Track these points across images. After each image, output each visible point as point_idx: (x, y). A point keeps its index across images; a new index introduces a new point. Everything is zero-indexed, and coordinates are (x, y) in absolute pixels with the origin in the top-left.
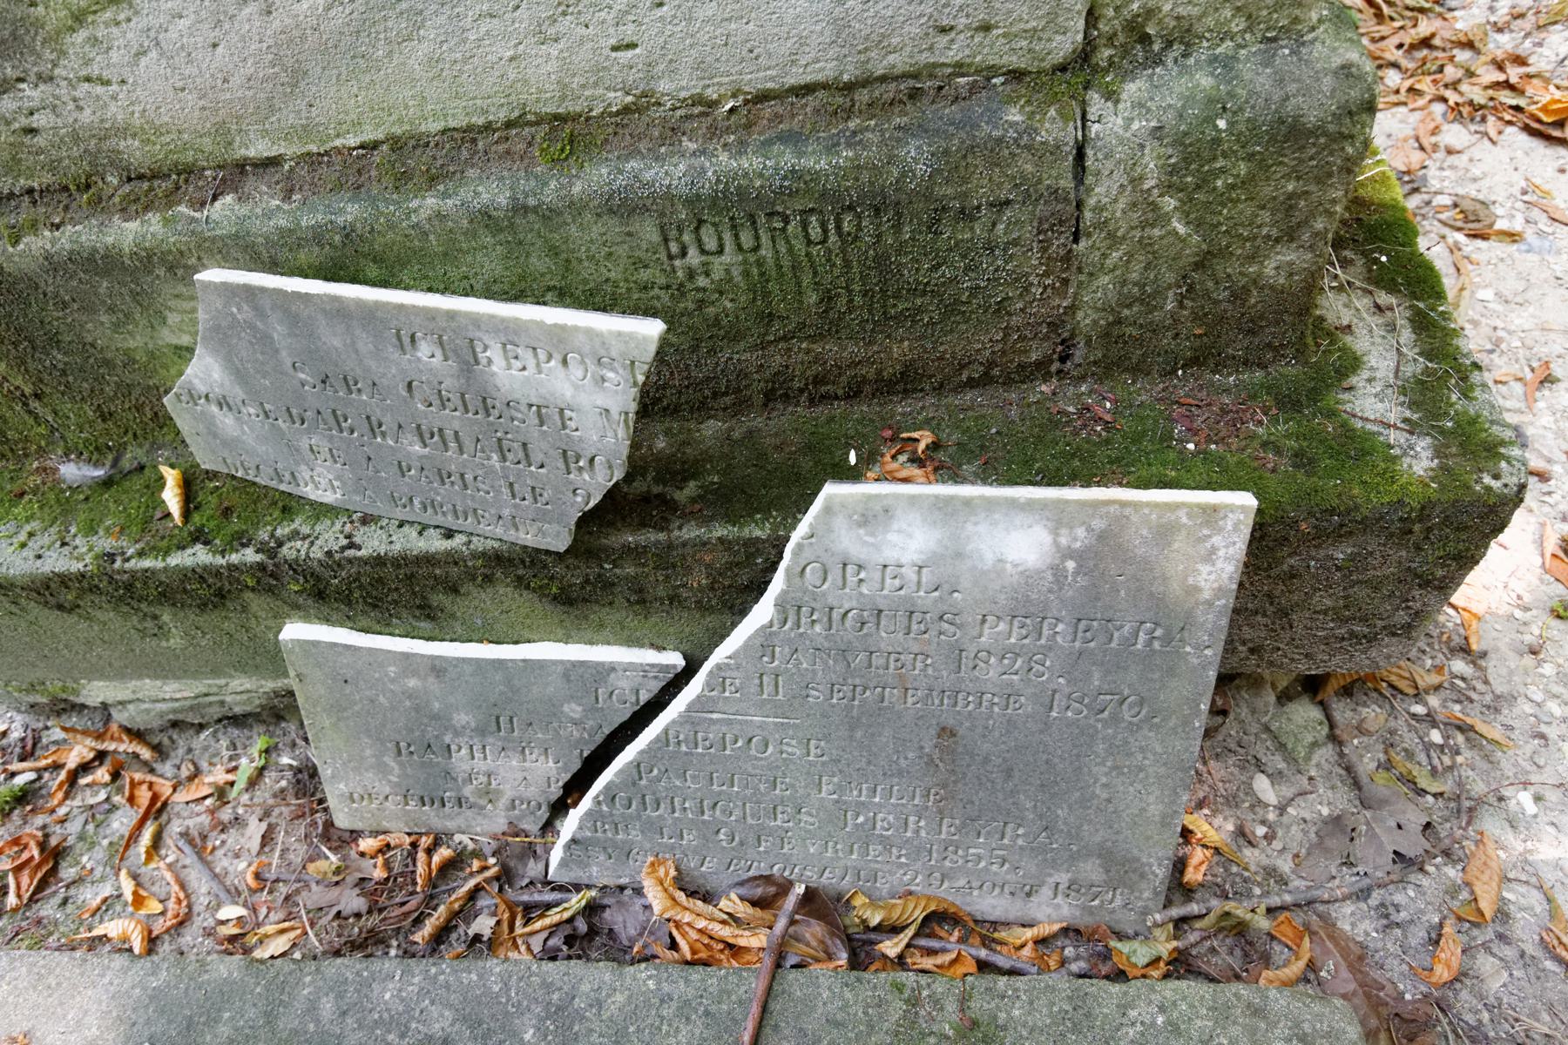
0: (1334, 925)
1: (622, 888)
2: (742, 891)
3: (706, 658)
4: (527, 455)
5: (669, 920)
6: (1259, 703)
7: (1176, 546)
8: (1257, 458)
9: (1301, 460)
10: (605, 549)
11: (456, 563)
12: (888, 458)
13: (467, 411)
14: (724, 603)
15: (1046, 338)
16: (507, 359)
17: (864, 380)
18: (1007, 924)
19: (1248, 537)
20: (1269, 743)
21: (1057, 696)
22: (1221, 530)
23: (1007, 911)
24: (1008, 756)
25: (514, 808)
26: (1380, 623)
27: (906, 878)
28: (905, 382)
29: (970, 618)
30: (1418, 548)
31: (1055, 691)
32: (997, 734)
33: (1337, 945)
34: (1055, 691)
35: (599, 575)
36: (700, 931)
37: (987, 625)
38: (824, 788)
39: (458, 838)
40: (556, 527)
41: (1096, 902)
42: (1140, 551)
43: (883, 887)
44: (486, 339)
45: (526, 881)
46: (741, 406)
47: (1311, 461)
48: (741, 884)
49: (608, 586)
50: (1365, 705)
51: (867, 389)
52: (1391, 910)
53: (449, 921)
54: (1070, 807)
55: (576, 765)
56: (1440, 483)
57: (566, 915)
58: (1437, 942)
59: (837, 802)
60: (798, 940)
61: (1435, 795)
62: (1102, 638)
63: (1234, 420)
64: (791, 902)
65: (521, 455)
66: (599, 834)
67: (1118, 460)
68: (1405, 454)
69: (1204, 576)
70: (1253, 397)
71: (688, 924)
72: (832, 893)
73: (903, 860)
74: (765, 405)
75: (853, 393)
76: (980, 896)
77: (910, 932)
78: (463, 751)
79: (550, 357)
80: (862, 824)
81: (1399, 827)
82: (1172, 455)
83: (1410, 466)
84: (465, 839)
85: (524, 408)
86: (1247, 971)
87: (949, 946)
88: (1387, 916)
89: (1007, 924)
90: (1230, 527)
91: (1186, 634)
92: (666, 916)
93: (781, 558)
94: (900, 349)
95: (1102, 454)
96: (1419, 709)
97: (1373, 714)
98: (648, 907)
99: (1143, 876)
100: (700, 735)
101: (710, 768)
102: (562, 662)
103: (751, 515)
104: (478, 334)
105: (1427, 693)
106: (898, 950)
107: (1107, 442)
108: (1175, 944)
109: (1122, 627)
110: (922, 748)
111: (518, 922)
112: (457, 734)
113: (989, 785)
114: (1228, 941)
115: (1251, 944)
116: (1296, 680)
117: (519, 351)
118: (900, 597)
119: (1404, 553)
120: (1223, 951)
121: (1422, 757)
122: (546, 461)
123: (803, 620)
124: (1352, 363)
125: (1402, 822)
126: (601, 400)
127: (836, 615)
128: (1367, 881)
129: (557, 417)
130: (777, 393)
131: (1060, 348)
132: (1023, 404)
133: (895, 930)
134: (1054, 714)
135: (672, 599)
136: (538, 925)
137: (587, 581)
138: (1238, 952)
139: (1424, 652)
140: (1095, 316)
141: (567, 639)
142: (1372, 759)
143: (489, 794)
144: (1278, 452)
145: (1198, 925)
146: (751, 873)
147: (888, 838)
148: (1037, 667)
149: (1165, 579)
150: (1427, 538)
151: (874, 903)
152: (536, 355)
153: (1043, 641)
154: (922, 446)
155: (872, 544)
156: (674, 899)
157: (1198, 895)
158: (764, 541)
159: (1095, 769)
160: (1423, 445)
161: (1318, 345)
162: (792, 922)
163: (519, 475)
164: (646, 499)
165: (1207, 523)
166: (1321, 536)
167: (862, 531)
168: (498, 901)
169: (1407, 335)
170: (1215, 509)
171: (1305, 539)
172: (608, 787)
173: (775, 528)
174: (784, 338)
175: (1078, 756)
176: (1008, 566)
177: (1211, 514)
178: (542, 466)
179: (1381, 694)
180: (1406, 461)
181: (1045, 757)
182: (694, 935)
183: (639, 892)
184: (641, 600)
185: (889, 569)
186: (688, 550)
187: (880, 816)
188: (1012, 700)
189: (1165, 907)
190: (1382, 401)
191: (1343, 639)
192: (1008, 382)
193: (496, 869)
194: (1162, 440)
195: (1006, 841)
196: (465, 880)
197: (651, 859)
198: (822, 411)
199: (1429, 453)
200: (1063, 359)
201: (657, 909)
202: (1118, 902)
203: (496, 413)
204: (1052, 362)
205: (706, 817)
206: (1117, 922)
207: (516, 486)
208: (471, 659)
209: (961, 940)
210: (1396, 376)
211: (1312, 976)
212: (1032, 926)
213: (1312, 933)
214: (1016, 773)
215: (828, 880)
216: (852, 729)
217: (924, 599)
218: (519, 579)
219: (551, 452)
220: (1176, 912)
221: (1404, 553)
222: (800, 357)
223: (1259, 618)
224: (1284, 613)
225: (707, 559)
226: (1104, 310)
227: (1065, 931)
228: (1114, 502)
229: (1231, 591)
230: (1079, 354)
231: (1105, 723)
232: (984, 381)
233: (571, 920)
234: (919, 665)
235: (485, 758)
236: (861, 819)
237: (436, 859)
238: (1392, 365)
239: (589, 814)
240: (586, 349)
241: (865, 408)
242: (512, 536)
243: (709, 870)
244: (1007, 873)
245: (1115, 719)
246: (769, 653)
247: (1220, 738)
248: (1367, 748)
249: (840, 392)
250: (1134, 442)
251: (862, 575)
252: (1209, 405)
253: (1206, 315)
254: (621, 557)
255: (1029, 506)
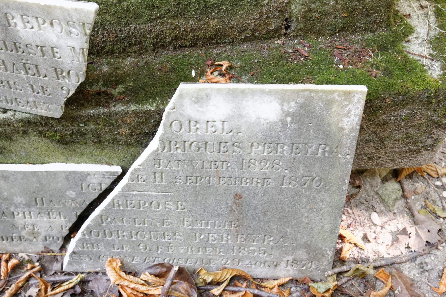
0: (402, 272)
1: (97, 273)
2: (151, 271)
3: (130, 167)
4: (38, 71)
5: (118, 285)
6: (374, 183)
7: (334, 109)
8: (369, 71)
9: (387, 72)
10: (80, 117)
11: (9, 125)
12: (209, 73)
13: (7, 50)
14: (138, 142)
15: (278, 18)
16: (24, 23)
17: (198, 38)
18: (267, 279)
19: (364, 105)
20: (378, 200)
21: (285, 178)
22: (352, 102)
23: (267, 274)
24: (265, 205)
25: (46, 240)
26: (421, 145)
27: (223, 262)
28: (216, 39)
29: (247, 145)
30: (435, 110)
31: (284, 176)
32: (260, 196)
33: (402, 280)
34: (284, 176)
35: (78, 130)
36: (132, 289)
37: (254, 148)
38: (186, 223)
39: (20, 255)
40: (54, 106)
41: (304, 268)
42: (319, 112)
43: (213, 266)
44: (14, 13)
45: (53, 272)
46: (142, 51)
47: (391, 72)
48: (150, 268)
49: (84, 134)
50: (417, 182)
51: (200, 42)
52: (424, 265)
53: (17, 291)
54: (292, 227)
55: (74, 219)
56: (443, 81)
57: (71, 285)
58: (441, 277)
59: (192, 229)
60: (176, 290)
61: (443, 218)
62: (303, 152)
63: (359, 54)
64: (172, 274)
65: (35, 71)
66: (85, 249)
67: (310, 73)
68: (429, 69)
69: (346, 123)
70: (368, 45)
71: (127, 286)
72: (191, 270)
73: (221, 254)
74: (154, 50)
75: (194, 45)
76: (255, 268)
77: (225, 284)
78: (20, 215)
79: (44, 22)
80: (203, 239)
81: (429, 231)
82: (333, 71)
83: (431, 74)
84: (24, 255)
85: (34, 47)
86: (366, 292)
87: (241, 289)
88: (423, 268)
89: (267, 279)
90: (356, 101)
91: (339, 149)
92: (117, 283)
93: (162, 119)
94: (213, 23)
95: (303, 70)
96: (439, 183)
97: (420, 186)
98: (108, 280)
99: (323, 255)
100: (128, 202)
101: (135, 216)
102: (64, 172)
103: (147, 100)
104: (9, 11)
105: (442, 177)
106: (220, 292)
107: (306, 65)
108: (336, 283)
109: (312, 147)
110: (227, 204)
111: (49, 289)
112: (16, 206)
113: (257, 219)
114: (358, 281)
115: (368, 281)
116: (389, 173)
117: (29, 19)
118: (215, 136)
119: (429, 113)
120: (356, 285)
121: (439, 203)
122: (48, 74)
123: (172, 147)
124: (410, 31)
125: (430, 230)
126: (71, 43)
127: (187, 145)
128: (415, 254)
129: (50, 52)
130: (159, 45)
131: (285, 23)
132: (270, 49)
133: (219, 284)
134: (284, 186)
135: (113, 141)
136: (58, 290)
137: (73, 133)
138: (362, 285)
139: (441, 160)
140: (299, 7)
141: (66, 161)
142: (419, 205)
143: (34, 234)
144: (377, 69)
145: (346, 275)
146: (155, 263)
147: (214, 244)
148: (276, 165)
149: (329, 125)
150: (438, 106)
151: (209, 273)
152: (37, 21)
153: (278, 154)
154: (224, 68)
155: (202, 112)
156: (120, 276)
157: (347, 263)
158: (153, 112)
159: (302, 210)
160: (437, 65)
161: (396, 22)
162: (173, 283)
163: (35, 81)
164: (99, 93)
165: (346, 99)
166: (396, 105)
167: (196, 106)
168: (39, 280)
169: (433, 18)
170: (350, 93)
171: (388, 107)
172: (88, 228)
173: (158, 105)
174: (160, 17)
175: (295, 204)
176: (262, 121)
177: (348, 94)
178: (46, 76)
179: (424, 177)
180: (430, 72)
181: (281, 206)
182: (129, 291)
183: (104, 274)
184: (99, 142)
185: (209, 123)
186: (119, 117)
187: (211, 235)
188: (266, 181)
189: (333, 268)
190: (421, 47)
191: (406, 152)
192: (263, 39)
193: (39, 267)
194: (329, 64)
195: (265, 243)
196: (24, 273)
197: (109, 259)
198: (180, 53)
199: (439, 69)
200: (287, 28)
201: (112, 280)
202: (313, 267)
203: (21, 50)
204: (282, 29)
205: (133, 239)
206: (313, 276)
207: (34, 86)
208: (21, 172)
209: (247, 287)
210: (428, 36)
211: (392, 294)
212: (277, 279)
213: (392, 276)
214: (269, 213)
215: (189, 265)
216: (196, 196)
217: (226, 137)
218: (40, 132)
219: (49, 69)
220: (337, 270)
221: (429, 113)
222: (166, 27)
223: (372, 144)
224: (382, 141)
225: (128, 120)
226: (303, 4)
227: (291, 280)
228: (307, 90)
229: (357, 129)
230: (293, 25)
231: (306, 190)
232: (252, 39)
233: (73, 288)
234: (225, 166)
235: (31, 218)
236: (202, 237)
237: (10, 264)
238: (426, 31)
239: (80, 240)
240: (61, 17)
241: (199, 51)
242: (34, 111)
243: (136, 263)
244: (266, 257)
245: (310, 187)
246: (158, 163)
247: (358, 198)
248: (417, 200)
249: (188, 44)
250: (317, 65)
251: (198, 126)
252: (349, 49)
253: (347, 7)
254: (88, 121)
255: (270, 93)
